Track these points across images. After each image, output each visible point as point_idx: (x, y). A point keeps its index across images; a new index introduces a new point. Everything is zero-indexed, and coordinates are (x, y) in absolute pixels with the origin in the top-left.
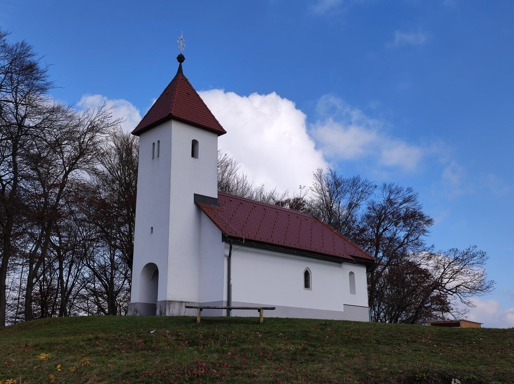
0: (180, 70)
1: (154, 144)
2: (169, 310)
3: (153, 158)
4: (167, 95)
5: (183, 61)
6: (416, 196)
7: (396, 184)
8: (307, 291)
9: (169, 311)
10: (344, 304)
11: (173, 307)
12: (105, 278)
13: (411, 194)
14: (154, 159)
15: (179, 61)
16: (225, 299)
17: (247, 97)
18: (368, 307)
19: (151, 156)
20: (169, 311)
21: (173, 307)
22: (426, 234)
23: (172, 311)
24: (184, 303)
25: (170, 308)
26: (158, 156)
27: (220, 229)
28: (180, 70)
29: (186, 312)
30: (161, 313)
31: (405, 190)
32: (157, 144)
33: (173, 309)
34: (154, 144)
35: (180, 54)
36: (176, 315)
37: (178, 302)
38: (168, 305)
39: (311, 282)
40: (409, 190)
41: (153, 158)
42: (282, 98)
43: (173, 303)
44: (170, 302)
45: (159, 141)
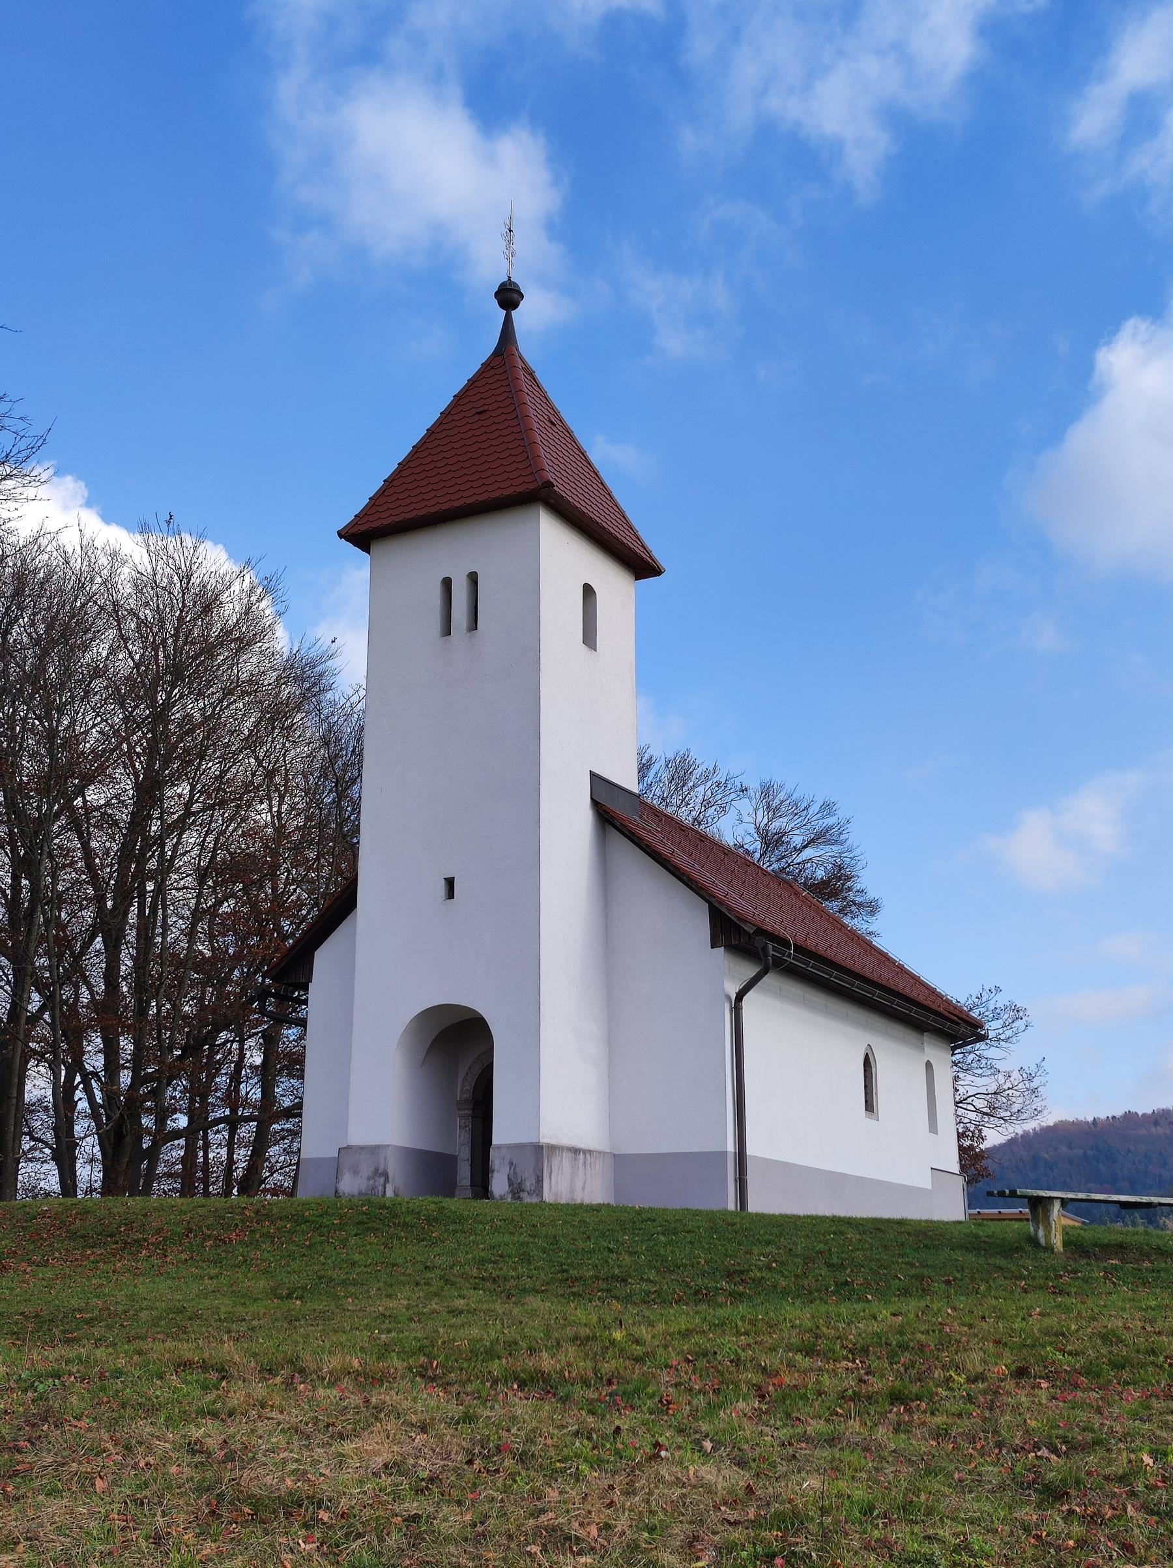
0: (507, 331)
1: (447, 583)
2: (551, 1179)
3: (447, 631)
4: (477, 417)
5: (515, 305)
6: (842, 829)
7: (789, 787)
8: (871, 1122)
13: (830, 821)
15: (503, 305)
16: (731, 1147)
18: (957, 1170)
26: (474, 624)
28: (507, 331)
29: (586, 1185)
30: (516, 1189)
31: (814, 809)
33: (558, 1175)
34: (447, 583)
35: (506, 279)
36: (563, 1201)
39: (876, 1094)
40: (828, 808)
41: (447, 631)
42: (215, 545)
44: (553, 1148)
45: (473, 578)
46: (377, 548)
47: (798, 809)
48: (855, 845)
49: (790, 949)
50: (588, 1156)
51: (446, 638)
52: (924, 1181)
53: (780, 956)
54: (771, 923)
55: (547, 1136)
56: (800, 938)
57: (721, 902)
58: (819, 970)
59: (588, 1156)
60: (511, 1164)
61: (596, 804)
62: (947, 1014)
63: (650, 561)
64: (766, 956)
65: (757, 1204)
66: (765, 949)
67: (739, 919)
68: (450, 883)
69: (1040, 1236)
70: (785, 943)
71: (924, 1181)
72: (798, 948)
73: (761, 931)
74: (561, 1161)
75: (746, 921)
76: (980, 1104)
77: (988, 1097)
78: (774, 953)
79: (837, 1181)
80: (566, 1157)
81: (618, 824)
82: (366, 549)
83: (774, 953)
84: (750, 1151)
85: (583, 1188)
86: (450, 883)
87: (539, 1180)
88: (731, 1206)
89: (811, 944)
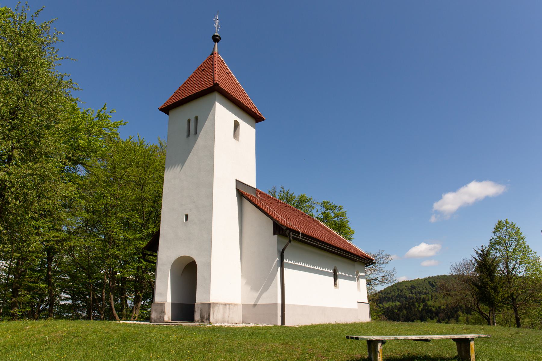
1: (189, 121)
3: (188, 135)
9: (214, 316)
10: (358, 302)
11: (217, 311)
12: (478, 311)
14: (189, 136)
16: (279, 302)
17: (399, 282)
18: (367, 302)
19: (185, 134)
20: (214, 316)
21: (217, 311)
22: (492, 232)
23: (217, 315)
24: (228, 305)
25: (214, 312)
27: (272, 220)
32: (194, 120)
34: (189, 121)
37: (222, 304)
38: (213, 309)
41: (188, 135)
43: (217, 305)
45: (196, 118)
46: (171, 113)
47: (332, 208)
48: (348, 217)
49: (300, 235)
50: (231, 306)
51: (188, 138)
52: (355, 306)
53: (296, 237)
54: (294, 227)
55: (212, 300)
56: (303, 232)
57: (275, 220)
58: (314, 243)
59: (231, 306)
60: (201, 310)
61: (237, 190)
62: (361, 256)
63: (259, 115)
64: (290, 237)
65: (288, 323)
66: (289, 234)
67: (281, 225)
68: (187, 216)
69: (372, 358)
70: (298, 233)
71: (355, 306)
72: (303, 234)
73: (288, 229)
74: (219, 308)
75: (283, 225)
76: (380, 279)
77: (382, 278)
78: (293, 236)
79: (323, 310)
80: (221, 307)
81: (244, 196)
82: (167, 113)
83: (293, 236)
84: (286, 302)
85: (229, 317)
86: (187, 216)
87: (209, 315)
88: (279, 323)
89: (306, 232)
